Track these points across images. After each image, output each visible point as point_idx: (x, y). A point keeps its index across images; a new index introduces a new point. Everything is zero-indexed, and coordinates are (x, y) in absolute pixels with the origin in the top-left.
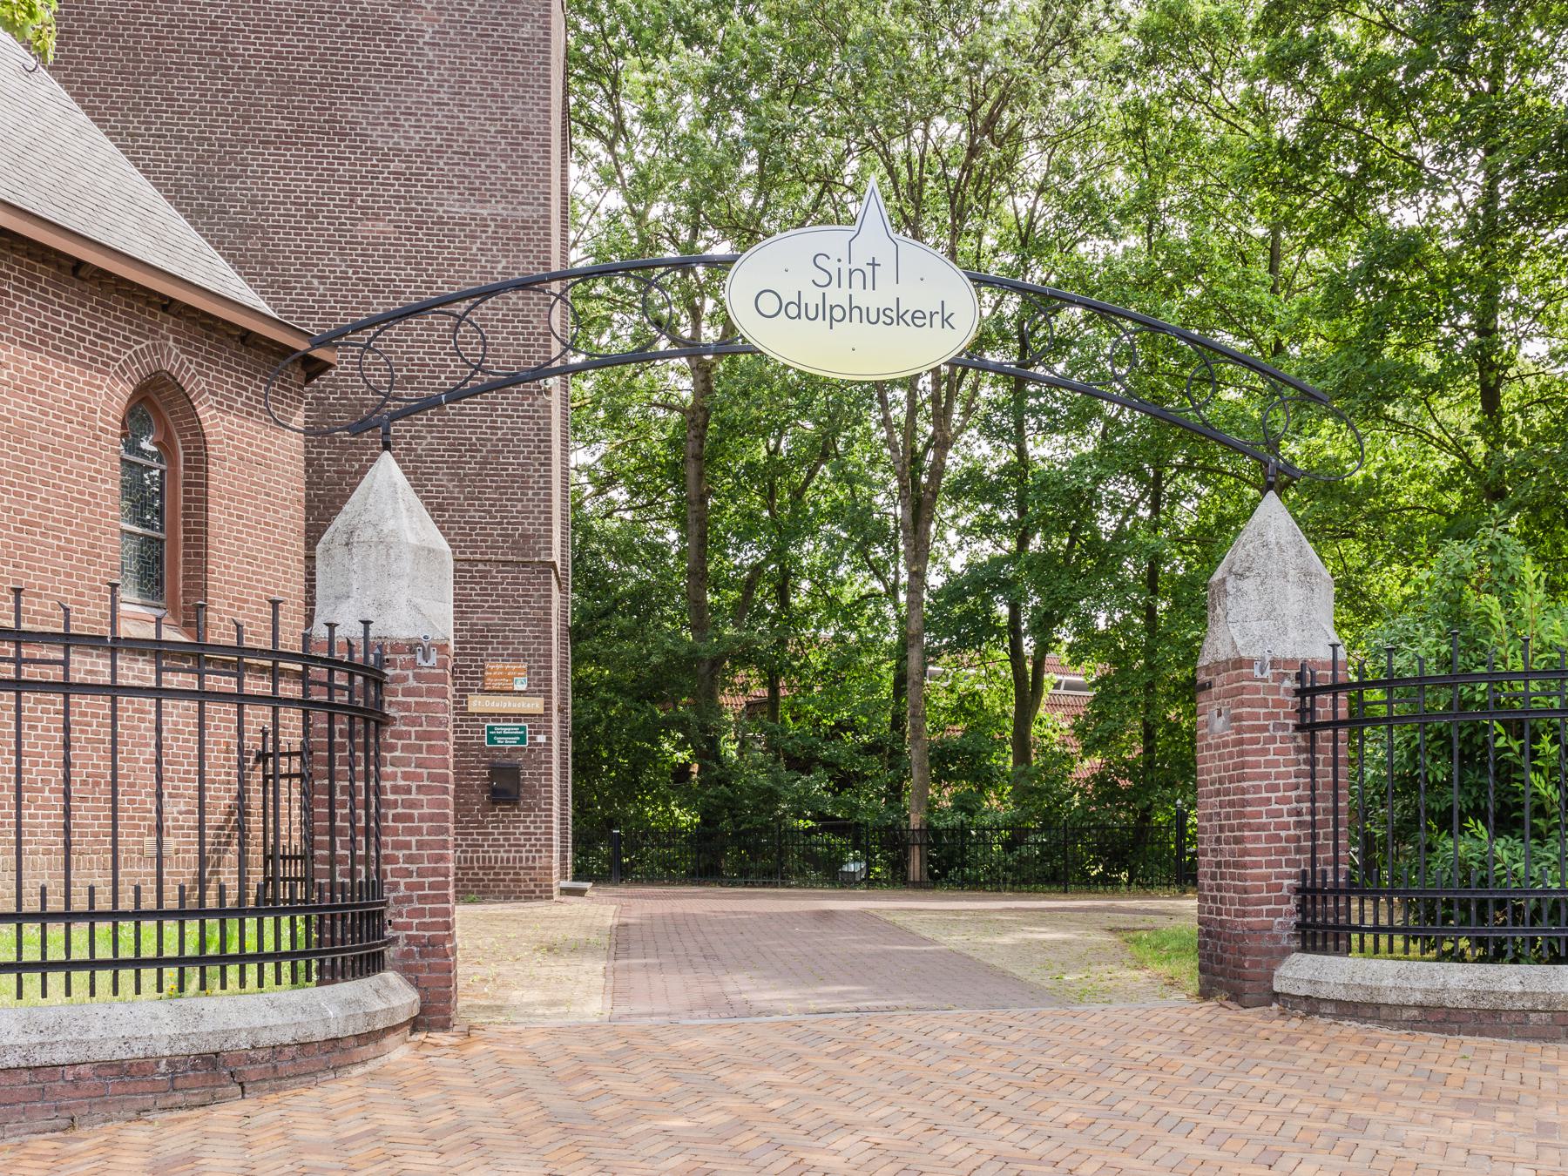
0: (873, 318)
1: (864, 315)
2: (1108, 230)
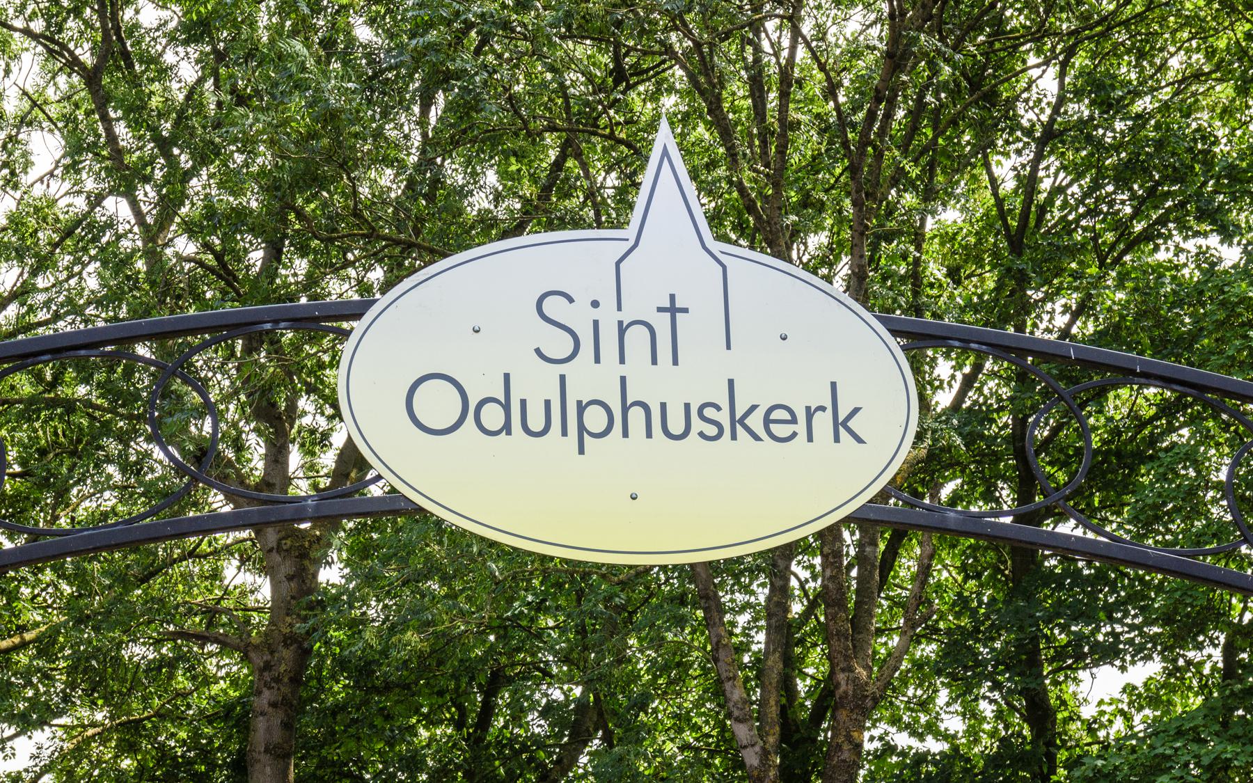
0: (676, 426)
1: (657, 421)
2: (1204, 214)
